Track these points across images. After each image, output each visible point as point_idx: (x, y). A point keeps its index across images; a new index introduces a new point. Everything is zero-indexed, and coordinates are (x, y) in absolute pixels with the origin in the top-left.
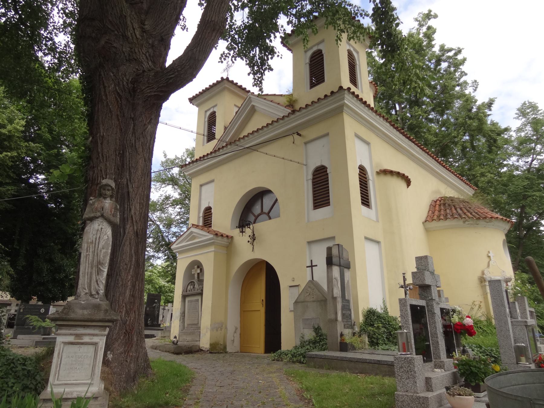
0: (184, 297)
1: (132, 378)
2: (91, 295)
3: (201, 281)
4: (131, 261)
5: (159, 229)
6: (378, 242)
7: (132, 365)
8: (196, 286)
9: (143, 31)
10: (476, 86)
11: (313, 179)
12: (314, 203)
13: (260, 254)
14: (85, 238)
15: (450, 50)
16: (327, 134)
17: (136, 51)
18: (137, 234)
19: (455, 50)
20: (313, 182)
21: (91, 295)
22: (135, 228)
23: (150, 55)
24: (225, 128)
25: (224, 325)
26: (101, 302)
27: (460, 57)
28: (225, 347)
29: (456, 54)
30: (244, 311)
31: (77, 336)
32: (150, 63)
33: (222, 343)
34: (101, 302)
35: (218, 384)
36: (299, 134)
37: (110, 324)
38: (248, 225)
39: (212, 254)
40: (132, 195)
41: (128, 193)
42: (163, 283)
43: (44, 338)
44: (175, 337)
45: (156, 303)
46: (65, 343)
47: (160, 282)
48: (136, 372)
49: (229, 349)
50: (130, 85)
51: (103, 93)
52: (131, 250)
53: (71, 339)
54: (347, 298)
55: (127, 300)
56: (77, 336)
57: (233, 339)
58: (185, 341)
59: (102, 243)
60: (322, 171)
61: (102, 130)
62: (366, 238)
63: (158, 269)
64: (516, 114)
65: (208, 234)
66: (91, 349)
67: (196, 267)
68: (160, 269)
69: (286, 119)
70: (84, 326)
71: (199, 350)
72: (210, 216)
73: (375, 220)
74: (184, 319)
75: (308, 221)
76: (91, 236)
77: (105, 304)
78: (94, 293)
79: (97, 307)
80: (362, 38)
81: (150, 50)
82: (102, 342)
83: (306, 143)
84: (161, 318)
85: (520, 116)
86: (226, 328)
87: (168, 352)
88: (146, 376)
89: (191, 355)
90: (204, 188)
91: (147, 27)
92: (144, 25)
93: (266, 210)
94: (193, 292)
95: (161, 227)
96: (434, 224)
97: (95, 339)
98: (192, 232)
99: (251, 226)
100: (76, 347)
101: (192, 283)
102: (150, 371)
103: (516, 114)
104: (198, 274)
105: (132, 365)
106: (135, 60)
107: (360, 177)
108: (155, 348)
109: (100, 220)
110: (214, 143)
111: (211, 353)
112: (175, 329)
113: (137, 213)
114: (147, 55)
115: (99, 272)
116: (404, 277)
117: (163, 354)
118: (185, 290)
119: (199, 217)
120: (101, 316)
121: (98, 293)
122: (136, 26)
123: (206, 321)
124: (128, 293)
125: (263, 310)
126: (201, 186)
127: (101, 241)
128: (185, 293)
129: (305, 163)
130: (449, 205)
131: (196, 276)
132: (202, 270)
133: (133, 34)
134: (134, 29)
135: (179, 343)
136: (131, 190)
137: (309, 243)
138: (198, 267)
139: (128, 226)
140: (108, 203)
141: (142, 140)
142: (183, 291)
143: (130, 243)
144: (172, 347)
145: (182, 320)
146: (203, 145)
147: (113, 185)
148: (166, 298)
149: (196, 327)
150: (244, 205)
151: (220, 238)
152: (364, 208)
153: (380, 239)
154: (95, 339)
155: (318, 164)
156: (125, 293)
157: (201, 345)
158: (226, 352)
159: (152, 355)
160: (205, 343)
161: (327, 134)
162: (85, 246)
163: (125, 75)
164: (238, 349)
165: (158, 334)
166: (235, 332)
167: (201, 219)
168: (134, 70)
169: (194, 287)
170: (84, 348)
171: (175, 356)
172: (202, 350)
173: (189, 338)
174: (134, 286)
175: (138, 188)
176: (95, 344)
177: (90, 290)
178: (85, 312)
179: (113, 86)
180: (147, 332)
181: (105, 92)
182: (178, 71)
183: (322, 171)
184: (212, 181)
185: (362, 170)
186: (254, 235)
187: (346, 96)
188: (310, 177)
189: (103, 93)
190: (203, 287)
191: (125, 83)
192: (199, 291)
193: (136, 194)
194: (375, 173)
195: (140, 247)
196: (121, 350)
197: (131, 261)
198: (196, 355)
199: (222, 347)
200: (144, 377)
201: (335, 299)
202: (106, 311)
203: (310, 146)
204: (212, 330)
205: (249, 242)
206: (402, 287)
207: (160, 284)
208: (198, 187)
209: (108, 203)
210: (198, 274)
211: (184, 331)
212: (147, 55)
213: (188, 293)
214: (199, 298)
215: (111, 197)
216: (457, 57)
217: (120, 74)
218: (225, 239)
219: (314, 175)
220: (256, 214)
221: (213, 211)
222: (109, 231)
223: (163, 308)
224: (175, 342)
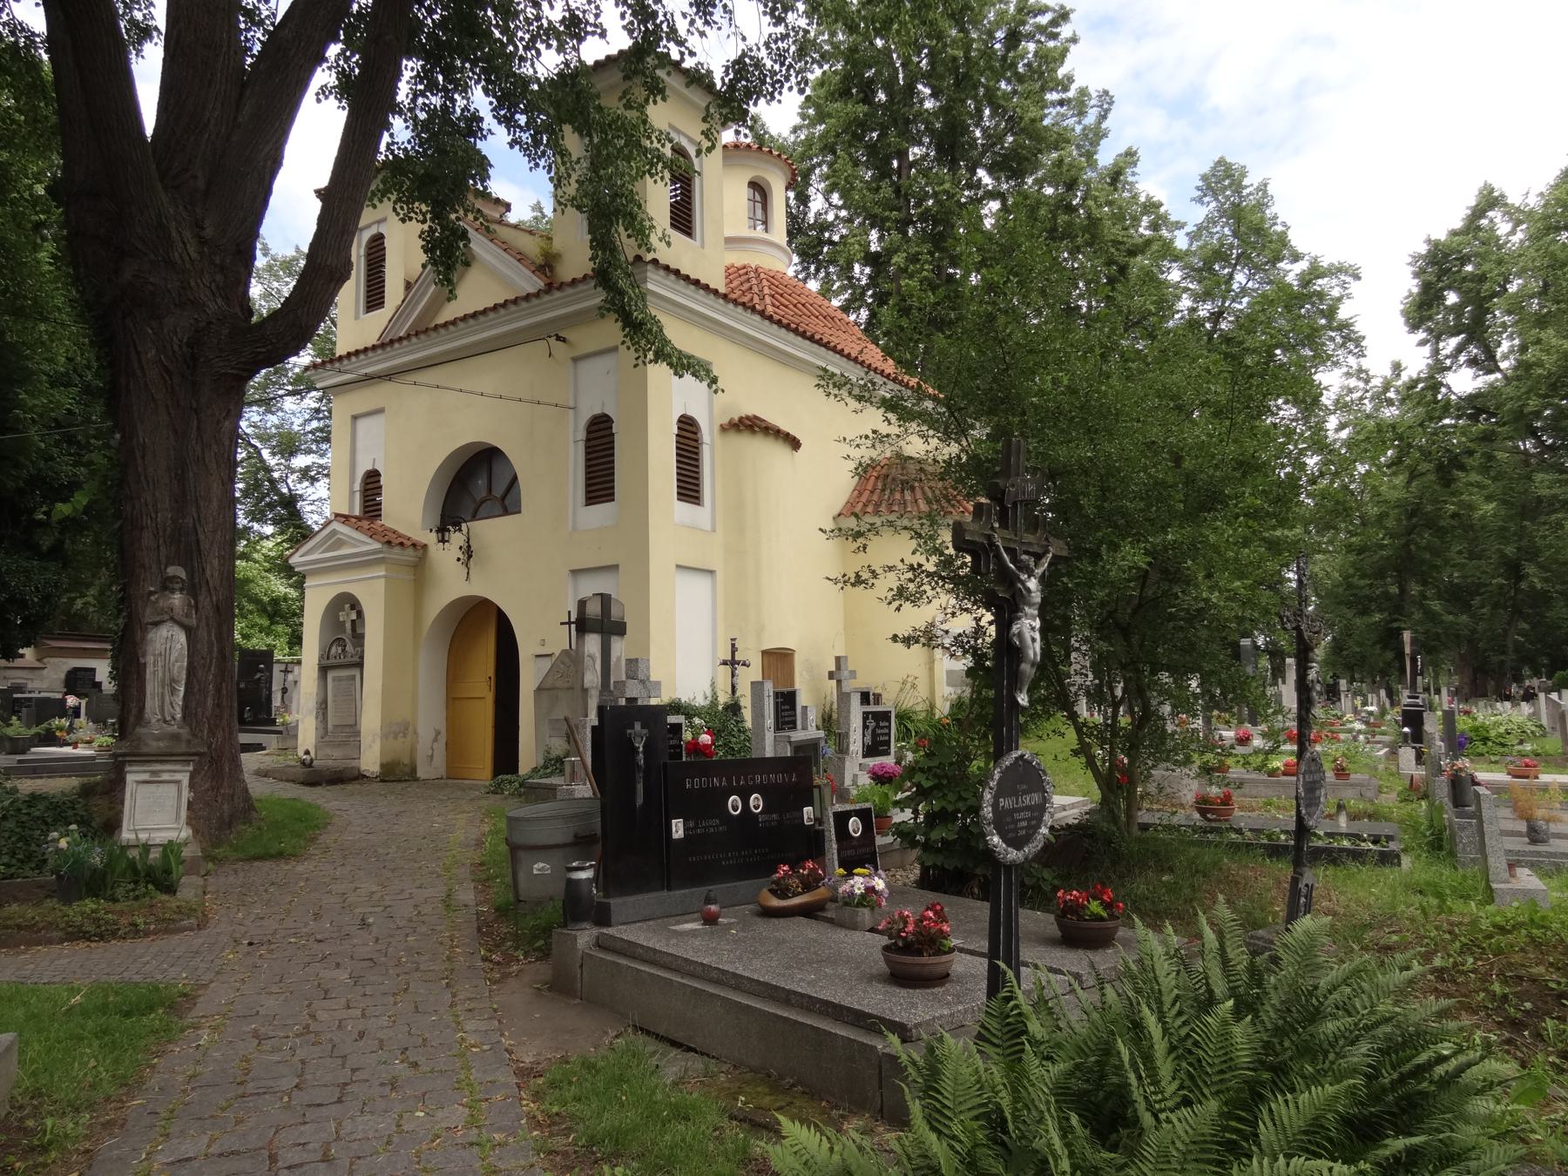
0: (324, 670)
1: (227, 824)
2: (165, 721)
3: (358, 638)
4: (210, 652)
5: (262, 461)
6: (712, 572)
7: (225, 807)
8: (349, 648)
9: (202, 241)
10: (1105, 106)
11: (588, 440)
12: (588, 492)
13: (478, 589)
14: (150, 650)
15: (1043, 10)
17: (193, 284)
18: (217, 609)
19: (1055, 11)
20: (587, 447)
21: (165, 721)
22: (214, 599)
23: (218, 287)
24: (408, 286)
25: (410, 729)
26: (181, 731)
27: (1065, 31)
28: (414, 770)
29: (1054, 23)
30: (454, 699)
31: (153, 773)
32: (219, 301)
33: (406, 761)
34: (181, 731)
35: (366, 830)
36: (559, 338)
37: (196, 758)
38: (457, 525)
40: (205, 545)
41: (198, 541)
42: (283, 590)
43: (20, 761)
44: (307, 753)
45: (261, 671)
46: (138, 782)
47: (273, 588)
48: (232, 816)
49: (421, 774)
50: (185, 349)
51: (136, 365)
52: (209, 635)
53: (146, 777)
55: (208, 713)
56: (153, 773)
57: (430, 753)
58: (331, 759)
59: (174, 655)
60: (602, 426)
61: (141, 434)
62: (678, 566)
63: (264, 551)
64: (1198, 188)
65: (369, 540)
66: (173, 789)
67: (347, 606)
68: (270, 550)
69: (535, 301)
70: (161, 762)
71: (359, 777)
72: (375, 491)
73: (708, 528)
74: (325, 715)
75: (574, 529)
76: (158, 645)
77: (185, 732)
78: (168, 718)
79: (175, 737)
81: (219, 277)
82: (185, 779)
83: (575, 360)
84: (276, 701)
85: (1205, 195)
86: (415, 732)
87: (293, 781)
88: (248, 821)
89: (339, 787)
90: (362, 424)
91: (209, 232)
92: (203, 229)
93: (498, 491)
94: (342, 660)
95: (266, 454)
97: (178, 777)
98: (334, 532)
99: (464, 526)
100: (152, 787)
101: (339, 641)
102: (255, 815)
103: (1198, 188)
104: (353, 622)
105: (225, 807)
106: (192, 302)
107: (694, 429)
108: (263, 774)
109: (169, 624)
110: (381, 317)
111: (382, 781)
112: (307, 737)
113: (216, 574)
114: (213, 287)
115: (173, 692)
116: (733, 645)
117: (282, 785)
118: (325, 654)
119: (352, 493)
120: (183, 748)
121: (174, 719)
122: (188, 234)
123: (371, 720)
124: (210, 702)
125: (490, 697)
126: (355, 418)
127: (173, 651)
128: (326, 662)
129: (571, 404)
130: (894, 479)
131: (348, 626)
132: (360, 614)
133: (185, 255)
134: (184, 243)
135: (315, 763)
136: (202, 537)
137: (575, 572)
138: (353, 607)
139: (201, 598)
140: (177, 599)
141: (214, 447)
142: (321, 657)
143: (208, 625)
144: (301, 770)
145: (321, 717)
146: (357, 318)
147: (183, 575)
148: (294, 631)
149: (351, 731)
150: (452, 475)
151: (397, 550)
152: (684, 509)
153: (716, 563)
154: (178, 777)
155: (597, 411)
156: (205, 702)
157: (363, 767)
158: (417, 780)
159: (258, 788)
160: (370, 762)
162: (150, 659)
163: (176, 333)
164: (442, 771)
165: (271, 741)
166: (435, 740)
167: (358, 498)
168: (192, 321)
169: (343, 650)
170: (163, 788)
171: (307, 789)
172: (365, 776)
173: (337, 753)
174: (218, 690)
175: (214, 532)
176: (178, 782)
177: (163, 714)
178: (161, 744)
179: (153, 352)
180: (245, 738)
181: (140, 361)
182: (272, 343)
183: (602, 426)
184: (380, 411)
185: (687, 427)
186: (469, 547)
187: (649, 274)
188: (582, 435)
189: (136, 365)
190: (363, 651)
191: (176, 348)
192: (356, 659)
193: (212, 544)
194: (717, 428)
195: (225, 628)
196: (207, 786)
197: (210, 652)
198: (350, 787)
199: (407, 769)
200: (245, 824)
201: (585, 691)
202: (189, 742)
203: (585, 367)
204: (384, 736)
205: (459, 560)
206: (725, 663)
207: (273, 592)
208: (349, 420)
209: (177, 599)
210: (353, 622)
211: (326, 739)
212: (213, 287)
213: (332, 661)
214: (356, 672)
215: (181, 590)
216: (1058, 30)
217: (165, 331)
218: (410, 551)
219: (589, 432)
220: (478, 499)
221: (383, 481)
222: (181, 638)
223: (283, 667)
224: (308, 762)
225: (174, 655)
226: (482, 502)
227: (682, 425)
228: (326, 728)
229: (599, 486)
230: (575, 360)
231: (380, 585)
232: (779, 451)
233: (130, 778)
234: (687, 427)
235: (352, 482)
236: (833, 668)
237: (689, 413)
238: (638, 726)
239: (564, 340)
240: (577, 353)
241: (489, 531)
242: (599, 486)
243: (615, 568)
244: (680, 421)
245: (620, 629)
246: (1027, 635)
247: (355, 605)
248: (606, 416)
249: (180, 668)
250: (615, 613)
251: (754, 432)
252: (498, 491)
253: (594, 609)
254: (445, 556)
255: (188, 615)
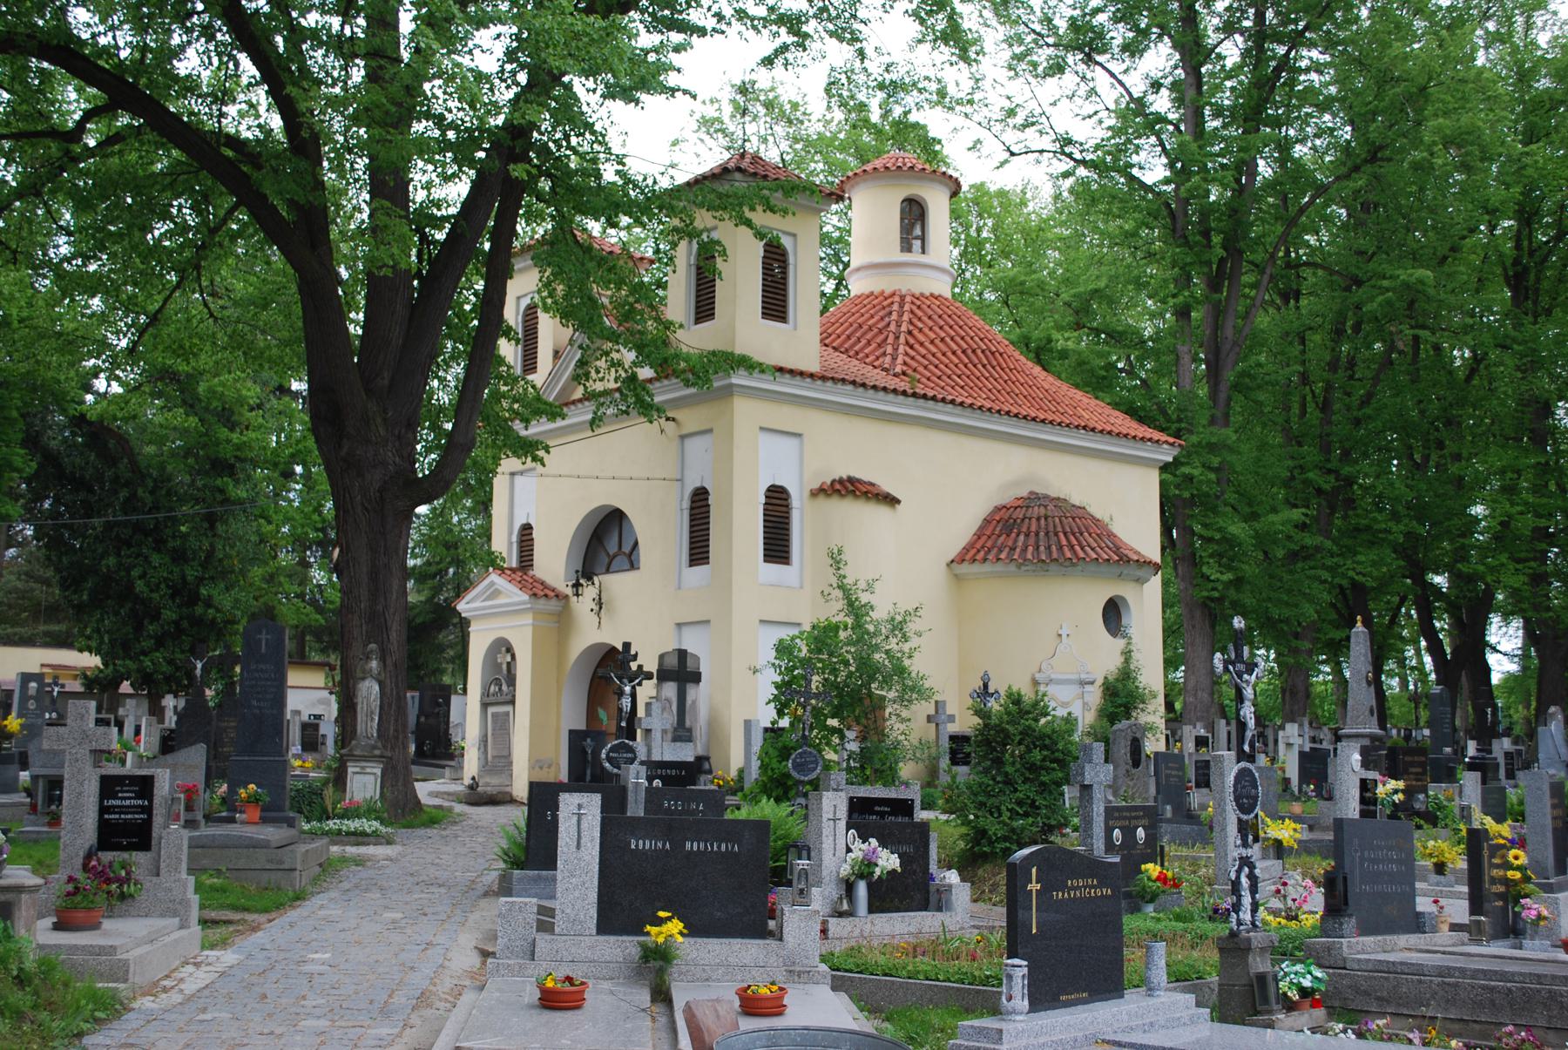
0: (485, 706)
3: (511, 680)
8: (504, 687)
11: (692, 509)
16: (710, 431)
24: (557, 355)
31: (363, 768)
39: (530, 628)
53: (358, 770)
54: (688, 724)
59: (373, 697)
62: (761, 621)
66: (372, 777)
74: (486, 746)
80: (325, 885)
82: (378, 772)
93: (627, 548)
94: (500, 699)
96: (965, 568)
97: (375, 770)
100: (361, 776)
101: (497, 682)
104: (508, 664)
107: (784, 496)
115: (372, 719)
118: (486, 693)
119: (511, 543)
128: (488, 700)
142: (483, 694)
152: (775, 569)
154: (375, 770)
161: (710, 431)
162: (359, 700)
170: (368, 777)
174: (396, 721)
194: (807, 493)
210: (508, 664)
213: (492, 699)
214: (509, 708)
219: (693, 502)
222: (377, 688)
225: (373, 697)
226: (615, 556)
227: (770, 494)
228: (486, 758)
229: (699, 552)
230: (683, 437)
231: (528, 632)
232: (880, 512)
233: (350, 770)
234: (777, 500)
235: (510, 534)
236: (932, 712)
237: (778, 483)
238: (589, 740)
239: (674, 420)
240: (685, 432)
241: (616, 583)
242: (699, 552)
243: (708, 622)
244: (769, 490)
245: (696, 678)
246: (1248, 716)
247: (509, 650)
248: (704, 488)
249: (375, 705)
250: (690, 664)
251: (856, 497)
252: (627, 548)
253: (673, 662)
254: (583, 605)
255: (379, 674)
